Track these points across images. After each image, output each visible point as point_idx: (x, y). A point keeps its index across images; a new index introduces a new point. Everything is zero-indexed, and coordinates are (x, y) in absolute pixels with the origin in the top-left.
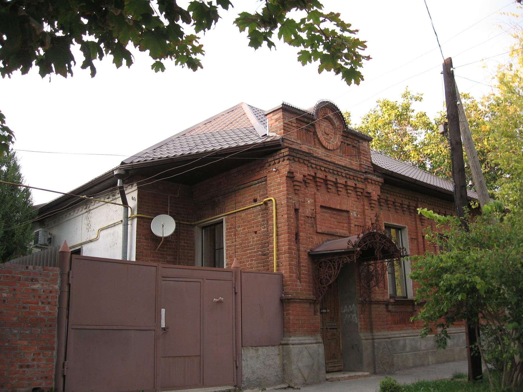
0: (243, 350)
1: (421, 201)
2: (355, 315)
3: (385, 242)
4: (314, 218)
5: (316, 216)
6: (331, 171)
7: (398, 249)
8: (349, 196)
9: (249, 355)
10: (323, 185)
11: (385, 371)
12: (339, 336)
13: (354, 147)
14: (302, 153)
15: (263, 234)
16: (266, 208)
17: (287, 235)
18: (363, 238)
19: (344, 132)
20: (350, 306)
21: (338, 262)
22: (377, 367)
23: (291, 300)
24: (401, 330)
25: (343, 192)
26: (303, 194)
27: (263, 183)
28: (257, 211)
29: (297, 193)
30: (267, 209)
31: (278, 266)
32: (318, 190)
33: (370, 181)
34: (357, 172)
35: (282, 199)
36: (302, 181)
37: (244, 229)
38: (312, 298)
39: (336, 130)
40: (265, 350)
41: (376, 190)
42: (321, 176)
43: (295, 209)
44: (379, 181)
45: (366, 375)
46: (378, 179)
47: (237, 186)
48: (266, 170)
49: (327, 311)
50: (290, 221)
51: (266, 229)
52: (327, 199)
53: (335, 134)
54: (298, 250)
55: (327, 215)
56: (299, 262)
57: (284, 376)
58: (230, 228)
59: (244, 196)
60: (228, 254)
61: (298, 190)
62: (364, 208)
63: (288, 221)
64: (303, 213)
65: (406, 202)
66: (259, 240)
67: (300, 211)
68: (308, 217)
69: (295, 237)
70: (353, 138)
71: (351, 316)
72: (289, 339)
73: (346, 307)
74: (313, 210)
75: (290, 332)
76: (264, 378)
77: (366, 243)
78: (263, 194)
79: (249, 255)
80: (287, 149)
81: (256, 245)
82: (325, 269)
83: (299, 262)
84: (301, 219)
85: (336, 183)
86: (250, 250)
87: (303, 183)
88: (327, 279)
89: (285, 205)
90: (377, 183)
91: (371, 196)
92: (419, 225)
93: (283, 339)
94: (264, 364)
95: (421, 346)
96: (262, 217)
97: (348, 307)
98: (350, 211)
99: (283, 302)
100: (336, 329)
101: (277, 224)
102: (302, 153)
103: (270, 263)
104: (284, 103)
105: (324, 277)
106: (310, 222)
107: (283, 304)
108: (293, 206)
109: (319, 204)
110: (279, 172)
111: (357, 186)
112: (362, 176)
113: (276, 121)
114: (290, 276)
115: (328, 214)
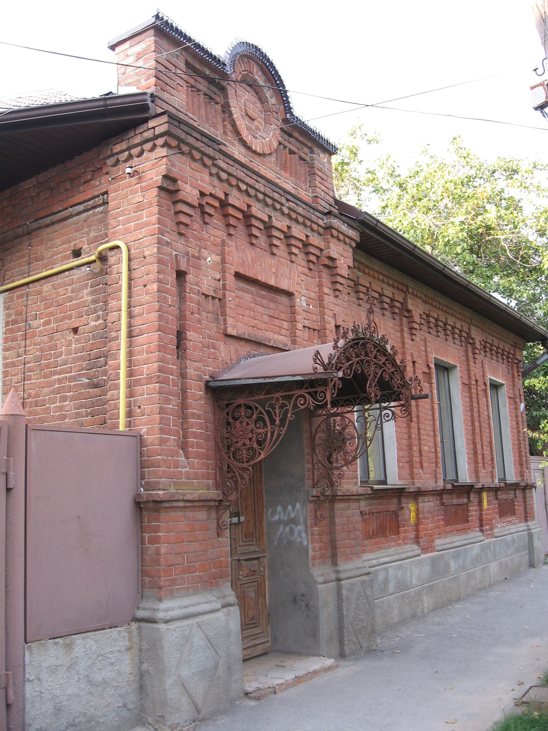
0: (27, 653)
1: (413, 294)
2: (301, 527)
3: (384, 364)
4: (220, 299)
5: (224, 295)
6: (261, 196)
7: (406, 381)
8: (293, 260)
9: (47, 665)
10: (241, 227)
11: (361, 647)
12: (263, 574)
13: (301, 159)
14: (199, 137)
15: (93, 335)
16: (102, 270)
17: (155, 336)
18: (345, 349)
19: (286, 121)
20: (290, 507)
21: (283, 406)
22: (346, 643)
23: (163, 505)
24: (379, 549)
25: (281, 251)
26: (196, 238)
27: (97, 210)
28: (79, 278)
29: (183, 232)
30: (104, 272)
31: (129, 414)
32: (230, 235)
33: (335, 233)
34: (312, 211)
35: (147, 244)
36: (196, 204)
37: (47, 323)
38: (214, 497)
39: (269, 115)
40: (92, 643)
41: (345, 256)
42: (237, 204)
43: (176, 271)
44: (352, 236)
45: (329, 668)
46: (351, 233)
47: (36, 220)
48: (108, 176)
49: (239, 519)
50: (165, 299)
51: (101, 321)
52: (250, 260)
53: (267, 122)
54: (183, 375)
55: (248, 297)
56: (184, 406)
57: (142, 705)
58: (15, 322)
59: (49, 244)
60: (8, 383)
61: (186, 225)
62: (321, 291)
63: (160, 300)
64: (197, 284)
65: (388, 292)
66: (83, 349)
67: (190, 277)
68: (207, 296)
69: (176, 341)
70: (302, 139)
71: (292, 531)
72: (156, 607)
73: (279, 508)
74: (219, 280)
75: (160, 588)
76: (89, 721)
77: (351, 362)
78: (96, 237)
79: (57, 386)
80: (165, 118)
81: (75, 360)
82: (248, 424)
83: (184, 406)
84: (190, 297)
85: (268, 227)
86: (60, 373)
87: (198, 211)
88: (252, 448)
89: (153, 259)
90: (347, 240)
91: (337, 267)
92: (408, 341)
93: (140, 606)
94: (89, 681)
95: (411, 579)
96: (91, 293)
97: (285, 509)
98: (295, 293)
99: (141, 508)
100: (258, 558)
101: (129, 306)
102: (199, 137)
103: (110, 405)
104: (160, 15)
105: (244, 444)
106: (210, 308)
107: (141, 512)
108: (172, 263)
109: (232, 269)
110: (140, 178)
111: (311, 242)
112: (320, 220)
113: (138, 59)
114: (162, 442)
115: (251, 296)
